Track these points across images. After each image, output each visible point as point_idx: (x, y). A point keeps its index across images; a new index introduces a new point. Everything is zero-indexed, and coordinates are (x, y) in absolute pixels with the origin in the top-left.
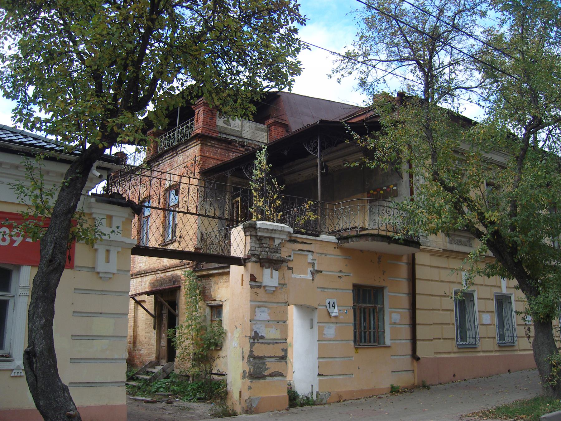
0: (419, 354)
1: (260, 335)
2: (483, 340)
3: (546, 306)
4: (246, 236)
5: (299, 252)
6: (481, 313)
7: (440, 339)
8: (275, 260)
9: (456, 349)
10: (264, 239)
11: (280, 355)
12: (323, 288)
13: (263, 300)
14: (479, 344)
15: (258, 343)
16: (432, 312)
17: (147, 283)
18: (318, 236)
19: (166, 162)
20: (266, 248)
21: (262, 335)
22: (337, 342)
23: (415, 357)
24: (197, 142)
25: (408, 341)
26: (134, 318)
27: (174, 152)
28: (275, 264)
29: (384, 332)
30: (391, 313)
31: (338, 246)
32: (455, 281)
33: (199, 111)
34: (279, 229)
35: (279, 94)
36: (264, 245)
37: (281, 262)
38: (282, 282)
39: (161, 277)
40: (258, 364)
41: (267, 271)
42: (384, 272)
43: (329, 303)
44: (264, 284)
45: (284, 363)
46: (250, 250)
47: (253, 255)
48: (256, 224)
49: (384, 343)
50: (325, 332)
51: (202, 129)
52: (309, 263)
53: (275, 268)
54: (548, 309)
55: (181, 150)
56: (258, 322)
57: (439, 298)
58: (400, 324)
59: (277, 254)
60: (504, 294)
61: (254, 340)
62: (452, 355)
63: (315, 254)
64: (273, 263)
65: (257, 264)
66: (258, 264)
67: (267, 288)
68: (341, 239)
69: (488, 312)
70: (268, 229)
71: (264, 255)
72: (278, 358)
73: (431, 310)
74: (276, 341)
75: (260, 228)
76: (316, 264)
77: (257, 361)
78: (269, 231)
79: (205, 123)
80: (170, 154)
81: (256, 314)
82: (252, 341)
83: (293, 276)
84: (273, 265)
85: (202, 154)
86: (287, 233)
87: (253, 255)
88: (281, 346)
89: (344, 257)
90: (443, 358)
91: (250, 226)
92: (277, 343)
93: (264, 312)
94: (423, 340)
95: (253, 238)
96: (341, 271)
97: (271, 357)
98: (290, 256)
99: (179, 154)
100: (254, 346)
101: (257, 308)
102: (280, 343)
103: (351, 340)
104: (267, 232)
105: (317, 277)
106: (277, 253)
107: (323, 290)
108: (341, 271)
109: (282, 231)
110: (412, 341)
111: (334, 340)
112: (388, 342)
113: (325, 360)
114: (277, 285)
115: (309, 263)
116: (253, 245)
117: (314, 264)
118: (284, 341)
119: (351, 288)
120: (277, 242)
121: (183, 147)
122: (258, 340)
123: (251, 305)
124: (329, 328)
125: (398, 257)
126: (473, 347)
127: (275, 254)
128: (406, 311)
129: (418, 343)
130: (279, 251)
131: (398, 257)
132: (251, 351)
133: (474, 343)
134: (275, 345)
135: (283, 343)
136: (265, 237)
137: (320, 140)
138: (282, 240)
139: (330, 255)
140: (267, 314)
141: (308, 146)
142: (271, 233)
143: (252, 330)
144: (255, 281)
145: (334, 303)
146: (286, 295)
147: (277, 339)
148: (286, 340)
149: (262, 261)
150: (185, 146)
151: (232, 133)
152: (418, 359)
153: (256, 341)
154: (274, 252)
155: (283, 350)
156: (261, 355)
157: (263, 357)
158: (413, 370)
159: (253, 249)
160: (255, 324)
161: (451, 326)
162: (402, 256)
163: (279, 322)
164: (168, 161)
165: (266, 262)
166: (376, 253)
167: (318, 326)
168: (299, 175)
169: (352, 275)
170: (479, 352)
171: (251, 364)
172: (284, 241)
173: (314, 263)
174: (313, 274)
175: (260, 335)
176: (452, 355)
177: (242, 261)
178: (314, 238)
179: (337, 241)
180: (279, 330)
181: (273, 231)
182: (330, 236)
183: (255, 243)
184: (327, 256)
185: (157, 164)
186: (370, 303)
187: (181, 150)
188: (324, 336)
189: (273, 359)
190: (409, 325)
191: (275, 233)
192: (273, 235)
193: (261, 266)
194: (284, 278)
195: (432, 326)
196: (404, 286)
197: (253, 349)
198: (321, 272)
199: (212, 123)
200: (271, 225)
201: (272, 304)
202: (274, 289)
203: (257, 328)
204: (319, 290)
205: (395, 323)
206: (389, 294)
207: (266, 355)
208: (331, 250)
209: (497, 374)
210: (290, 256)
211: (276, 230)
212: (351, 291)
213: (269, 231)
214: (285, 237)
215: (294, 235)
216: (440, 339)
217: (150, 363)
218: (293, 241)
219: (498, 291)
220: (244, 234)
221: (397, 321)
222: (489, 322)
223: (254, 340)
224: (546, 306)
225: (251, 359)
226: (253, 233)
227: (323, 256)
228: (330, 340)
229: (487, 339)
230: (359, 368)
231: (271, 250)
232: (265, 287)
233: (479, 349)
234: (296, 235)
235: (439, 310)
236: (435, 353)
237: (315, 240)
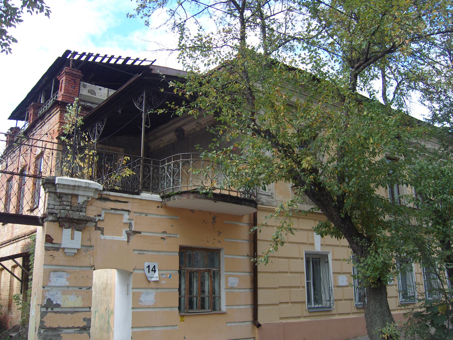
0: (260, 320)
1: (55, 303)
2: (338, 302)
3: (376, 269)
4: (46, 193)
5: (113, 211)
6: (336, 275)
7: (287, 303)
8: (78, 220)
9: (306, 314)
10: (65, 196)
11: (81, 326)
12: (141, 250)
13: (62, 263)
14: (334, 307)
15: (52, 312)
16: (278, 274)
17: (20, 248)
18: (138, 194)
19: (38, 132)
20: (67, 206)
21: (58, 302)
22: (158, 310)
23: (256, 324)
24: (57, 109)
25: (249, 307)
26: (10, 282)
27: (43, 121)
28: (77, 224)
29: (220, 297)
30: (227, 277)
31: (163, 206)
32: (306, 242)
33: (63, 81)
34: (83, 185)
35: (151, 67)
36: (65, 203)
37: (85, 222)
38: (88, 244)
39: (28, 242)
40: (50, 337)
41: (67, 232)
42: (220, 233)
43: (149, 267)
44: (63, 246)
45: (85, 334)
46: (48, 208)
47: (51, 214)
48: (54, 180)
49: (220, 309)
50: (142, 299)
51: (62, 97)
52: (125, 223)
53: (77, 228)
54: (378, 273)
55: (47, 118)
56: (54, 289)
57: (286, 260)
58: (239, 289)
59: (82, 214)
60: (319, 252)
61: (47, 309)
62: (302, 320)
63: (132, 214)
64: (74, 222)
65: (55, 223)
66: (57, 224)
67: (66, 251)
68: (165, 197)
69: (344, 273)
70: (69, 185)
71: (63, 213)
72: (79, 329)
73: (276, 273)
74: (75, 310)
75: (58, 184)
76: (133, 225)
77: (50, 333)
78: (71, 187)
79: (67, 91)
80: (40, 124)
81: (51, 279)
82: (44, 310)
83: (102, 237)
84: (75, 225)
85: (62, 121)
86: (94, 190)
87: (51, 214)
88: (83, 315)
89: (170, 217)
90: (290, 323)
91: (48, 181)
92: (77, 312)
93: (61, 277)
94: (267, 305)
95: (52, 195)
96: (164, 232)
97: (68, 328)
98: (100, 216)
99: (46, 122)
100: (46, 315)
101: (52, 273)
102: (82, 312)
103: (176, 307)
104: (68, 189)
105: (134, 238)
106: (81, 211)
107: (141, 252)
108: (164, 232)
109: (87, 188)
110: (253, 306)
111: (153, 308)
112: (224, 308)
113: (141, 330)
114: (79, 247)
115: (125, 223)
116: (52, 202)
117: (130, 224)
118: (88, 310)
119: (178, 250)
120: (81, 200)
121: (48, 116)
122: (52, 309)
123: (44, 269)
124: (147, 294)
125: (239, 218)
126: (328, 310)
127: (78, 213)
128: (248, 274)
129: (260, 309)
130: (84, 210)
131: (239, 218)
132: (42, 322)
133: (328, 305)
134: (75, 314)
135: (85, 311)
136: (66, 194)
137: (146, 95)
138: (88, 198)
139: (150, 214)
140: (65, 280)
141: (136, 101)
142: (74, 189)
143: (44, 297)
144: (52, 243)
145: (154, 267)
146: (92, 258)
147: (78, 307)
148: (90, 308)
149: (60, 220)
150: (49, 115)
151: (89, 100)
152: (259, 326)
153: (49, 310)
154: (78, 211)
155: (84, 319)
156: (55, 326)
157: (57, 328)
158: (255, 338)
159: (51, 207)
160: (48, 291)
161: (301, 289)
162: (243, 216)
163: (81, 288)
164: (39, 130)
165: (65, 222)
166: (210, 213)
167: (133, 293)
168: (161, 140)
169: (179, 236)
170: (335, 314)
171: (41, 337)
172: (90, 199)
173: (130, 223)
174: (129, 235)
175: (55, 303)
176: (302, 320)
177: (40, 221)
178: (131, 196)
179: (161, 200)
180: (80, 297)
181: (76, 188)
182: (153, 195)
183: (54, 200)
184: (149, 216)
185: (32, 134)
186: (203, 267)
187: (47, 118)
188: (140, 303)
189: (72, 331)
190: (251, 289)
191: (78, 190)
192: (76, 192)
193: (60, 226)
194: (90, 240)
195: (278, 290)
196: (246, 248)
197: (45, 319)
198: (140, 233)
199: (74, 91)
200: (72, 181)
201: (74, 268)
202: (76, 251)
203: (51, 295)
204: (136, 252)
205: (232, 288)
206: (225, 256)
207: (61, 326)
208: (153, 209)
209: (355, 337)
210: (100, 216)
211: (79, 187)
212: (178, 254)
213: (71, 187)
214: (91, 194)
215: (105, 193)
216: (287, 303)
217: (13, 327)
218: (102, 199)
219: (309, 249)
220: (44, 191)
221: (235, 286)
222: (345, 284)
223: (47, 309)
224: (376, 269)
225: (42, 331)
226: (52, 190)
227: (144, 215)
228: (148, 308)
229: (344, 302)
230: (185, 338)
231: (73, 208)
232: (64, 249)
233: (334, 312)
234: (108, 193)
235: (286, 272)
236: (280, 318)
237: (133, 198)
